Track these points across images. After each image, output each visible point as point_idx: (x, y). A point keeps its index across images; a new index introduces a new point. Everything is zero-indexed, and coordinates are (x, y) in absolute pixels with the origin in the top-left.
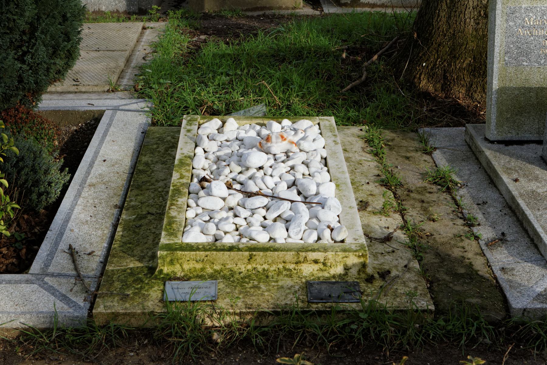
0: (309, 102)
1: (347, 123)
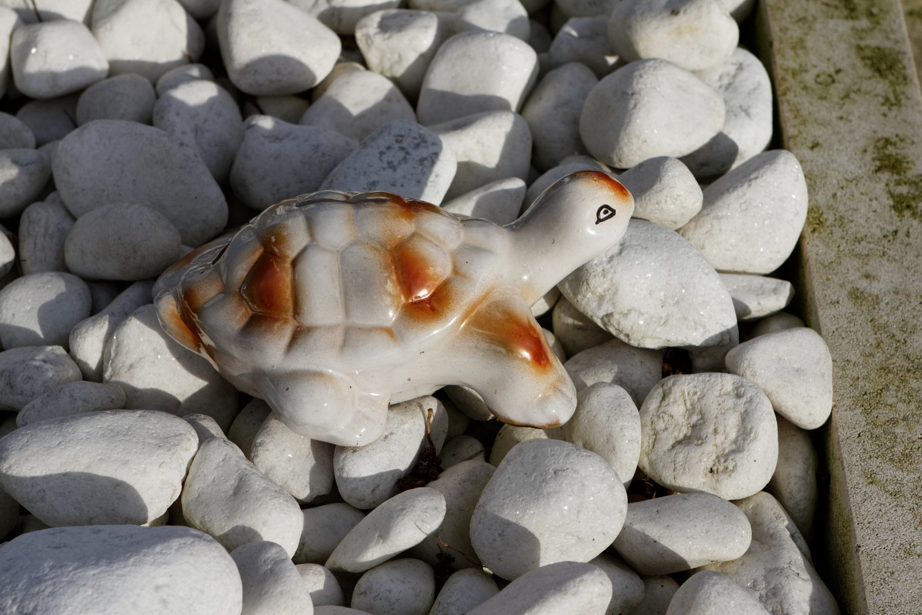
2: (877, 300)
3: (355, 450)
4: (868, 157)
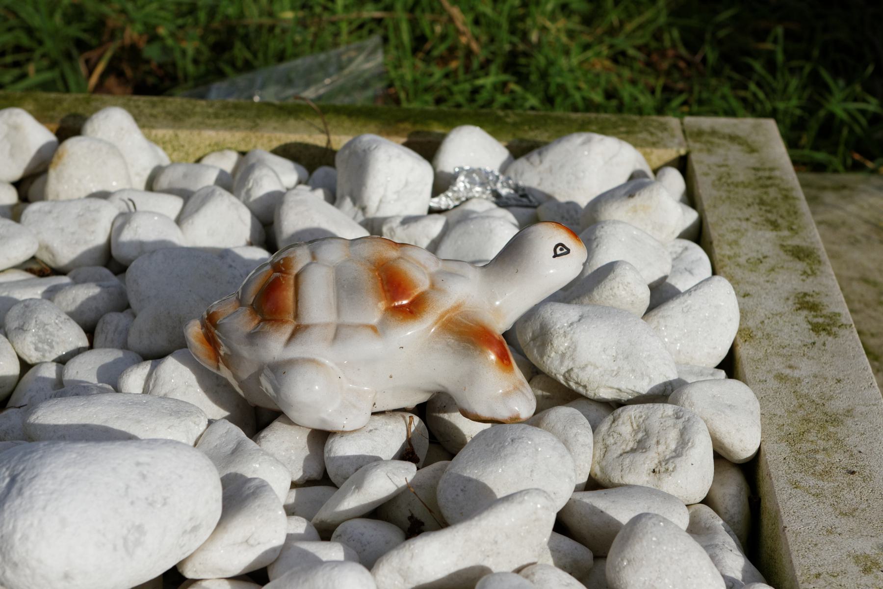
0: (621, 42)
1: (820, 156)
2: (799, 381)
3: (343, 433)
4: (790, 302)
